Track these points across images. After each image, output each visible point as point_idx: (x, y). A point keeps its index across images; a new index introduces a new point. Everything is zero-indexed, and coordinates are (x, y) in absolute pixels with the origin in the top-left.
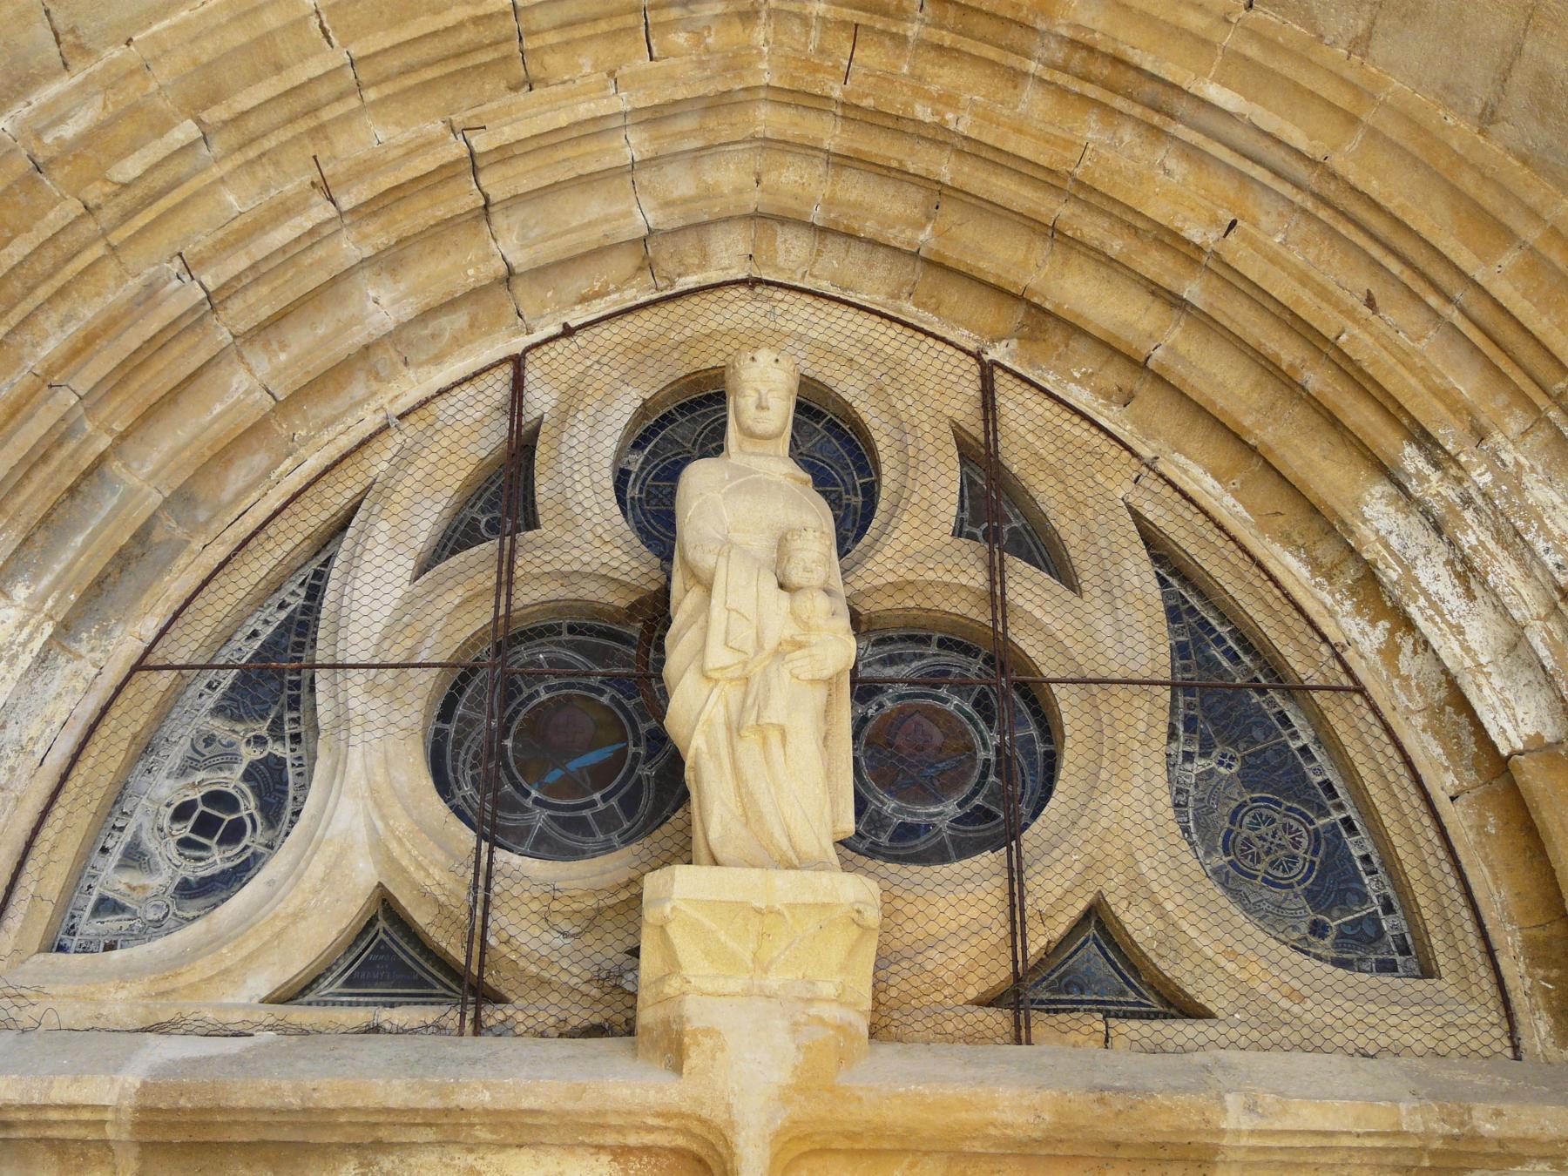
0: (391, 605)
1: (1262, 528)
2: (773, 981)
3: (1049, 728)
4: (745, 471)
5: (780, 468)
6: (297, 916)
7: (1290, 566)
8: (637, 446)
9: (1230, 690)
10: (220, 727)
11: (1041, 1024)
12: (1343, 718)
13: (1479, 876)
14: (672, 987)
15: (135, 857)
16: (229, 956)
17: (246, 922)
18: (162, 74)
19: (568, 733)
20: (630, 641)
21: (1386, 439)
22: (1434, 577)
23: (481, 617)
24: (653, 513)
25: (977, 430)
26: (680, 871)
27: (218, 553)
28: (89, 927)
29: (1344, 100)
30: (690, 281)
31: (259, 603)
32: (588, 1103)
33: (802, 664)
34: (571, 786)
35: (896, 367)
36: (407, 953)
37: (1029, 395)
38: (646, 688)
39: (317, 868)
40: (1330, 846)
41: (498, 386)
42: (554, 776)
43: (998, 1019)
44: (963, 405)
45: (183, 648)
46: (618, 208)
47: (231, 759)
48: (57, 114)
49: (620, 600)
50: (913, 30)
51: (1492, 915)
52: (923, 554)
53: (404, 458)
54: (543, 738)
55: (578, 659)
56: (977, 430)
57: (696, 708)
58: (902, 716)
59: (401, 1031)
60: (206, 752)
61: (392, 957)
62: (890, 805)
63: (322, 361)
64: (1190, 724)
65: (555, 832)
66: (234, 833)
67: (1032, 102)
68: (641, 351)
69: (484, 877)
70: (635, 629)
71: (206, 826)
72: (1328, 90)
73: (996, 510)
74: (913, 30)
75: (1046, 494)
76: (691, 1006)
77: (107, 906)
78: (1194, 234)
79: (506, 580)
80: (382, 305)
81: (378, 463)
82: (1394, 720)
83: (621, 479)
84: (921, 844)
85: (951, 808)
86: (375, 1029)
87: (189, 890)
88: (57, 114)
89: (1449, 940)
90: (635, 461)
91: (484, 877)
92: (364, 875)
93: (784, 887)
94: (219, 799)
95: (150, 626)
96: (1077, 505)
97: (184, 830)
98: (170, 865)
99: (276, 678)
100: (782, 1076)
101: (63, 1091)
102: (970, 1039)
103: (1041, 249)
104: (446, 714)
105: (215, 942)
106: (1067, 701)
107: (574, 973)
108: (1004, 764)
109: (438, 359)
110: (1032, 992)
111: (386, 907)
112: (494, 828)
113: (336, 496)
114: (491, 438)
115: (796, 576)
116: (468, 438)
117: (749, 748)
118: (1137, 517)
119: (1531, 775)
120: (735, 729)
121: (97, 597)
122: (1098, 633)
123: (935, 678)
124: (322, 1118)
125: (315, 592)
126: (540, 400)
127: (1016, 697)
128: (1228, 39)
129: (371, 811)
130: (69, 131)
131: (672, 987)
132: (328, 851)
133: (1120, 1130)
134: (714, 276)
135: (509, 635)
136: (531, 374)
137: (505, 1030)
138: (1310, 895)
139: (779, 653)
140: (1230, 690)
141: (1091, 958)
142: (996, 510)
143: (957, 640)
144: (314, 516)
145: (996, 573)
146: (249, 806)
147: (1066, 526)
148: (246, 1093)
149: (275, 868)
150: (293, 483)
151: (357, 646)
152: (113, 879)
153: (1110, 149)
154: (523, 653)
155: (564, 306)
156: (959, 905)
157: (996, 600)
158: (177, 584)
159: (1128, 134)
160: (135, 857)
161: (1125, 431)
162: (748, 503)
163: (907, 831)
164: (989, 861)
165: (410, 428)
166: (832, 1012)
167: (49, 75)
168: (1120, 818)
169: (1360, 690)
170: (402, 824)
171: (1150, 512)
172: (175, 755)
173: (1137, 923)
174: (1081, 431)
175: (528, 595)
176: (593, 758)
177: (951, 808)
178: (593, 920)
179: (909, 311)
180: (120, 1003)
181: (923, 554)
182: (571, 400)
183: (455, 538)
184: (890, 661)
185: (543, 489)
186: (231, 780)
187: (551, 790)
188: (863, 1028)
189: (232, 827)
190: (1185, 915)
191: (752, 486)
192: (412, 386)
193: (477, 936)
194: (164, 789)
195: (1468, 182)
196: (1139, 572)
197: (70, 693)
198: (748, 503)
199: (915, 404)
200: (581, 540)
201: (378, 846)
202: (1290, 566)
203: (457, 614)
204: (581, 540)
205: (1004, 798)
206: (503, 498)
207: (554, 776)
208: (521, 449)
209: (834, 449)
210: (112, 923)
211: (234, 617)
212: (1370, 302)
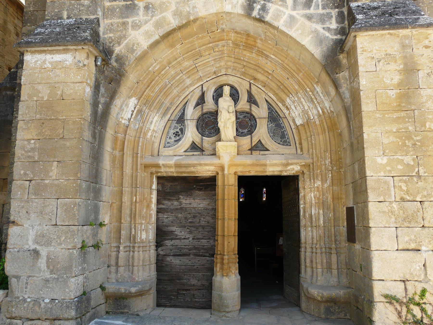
0: (192, 113)
1: (278, 101)
2: (228, 151)
3: (256, 122)
4: (225, 99)
5: (229, 99)
6: (185, 144)
7: (280, 105)
8: (215, 92)
9: (274, 118)
10: (176, 125)
11: (253, 152)
12: (285, 120)
13: (295, 136)
14: (219, 152)
15: (170, 138)
16: (180, 148)
17: (181, 145)
18: (165, 61)
19: (209, 124)
20: (215, 114)
21: (288, 93)
22: (293, 107)
23: (200, 113)
24: (217, 103)
25: (249, 90)
26: (219, 142)
27: (175, 108)
28: (167, 145)
29: (286, 56)
30: (219, 75)
31: (179, 112)
32: (212, 163)
33: (230, 121)
34: (210, 129)
35: (241, 83)
36: (196, 147)
37: (255, 86)
38: (216, 122)
39: (187, 140)
40: (283, 133)
41: (200, 87)
42: (208, 128)
43: (250, 152)
44: (248, 88)
45: (172, 118)
46: (211, 69)
47: (178, 128)
48: (155, 67)
49: (214, 111)
50: (241, 48)
51: (296, 140)
52: (243, 104)
53: (192, 96)
54: (207, 124)
55: (210, 116)
56: (249, 90)
57: (221, 125)
58: (242, 121)
59: (196, 155)
60: (175, 128)
61: (194, 147)
62: (240, 130)
63: (183, 88)
64: (270, 121)
65: (209, 134)
66: (179, 135)
67: (254, 55)
68: (215, 83)
69: (202, 139)
70: (215, 113)
71: (176, 135)
72: (284, 55)
73: (252, 100)
74: (241, 48)
75: (256, 97)
76: (220, 154)
77: (168, 143)
78: (270, 72)
79: (202, 110)
80: (188, 82)
81: (189, 97)
82: (289, 121)
83: (213, 96)
84: (243, 134)
85: (246, 130)
86: (193, 155)
87: (175, 141)
88: (155, 67)
89: (292, 143)
90: (215, 94)
91: (202, 139)
92: (191, 140)
93: (229, 143)
94: (177, 132)
95: (169, 116)
96: (259, 98)
97: (174, 135)
98: (173, 139)
99: (181, 119)
100: (229, 160)
101: (168, 163)
102: (247, 154)
103: (255, 71)
104: (197, 123)
105: (178, 147)
106: (257, 120)
107: (211, 149)
108: (251, 126)
109: (194, 85)
110: (252, 149)
111: (193, 142)
112: (203, 135)
113: (185, 101)
114: (200, 94)
115: (230, 111)
116: (198, 93)
117: (225, 129)
118: (265, 99)
119: (300, 128)
120: (224, 127)
121: (164, 114)
122: (261, 112)
123: (245, 117)
124: (190, 164)
125: (184, 110)
126: (205, 89)
127: (252, 118)
128: (274, 49)
129: (191, 134)
130: (156, 68)
131: (219, 152)
132: (188, 138)
133: (258, 163)
134: (222, 74)
135: (203, 115)
136: (203, 86)
137: (205, 155)
138: (281, 138)
139: (228, 120)
140: (274, 118)
141: (259, 145)
142: (252, 100)
143: (247, 113)
144: (183, 103)
145: (251, 106)
146: (180, 133)
147: (258, 100)
148: (183, 162)
149: (183, 139)
150: (181, 100)
151: (189, 118)
152: (169, 140)
153: (262, 61)
154: (205, 116)
155: (206, 78)
156: (246, 141)
157: (251, 109)
158: (171, 111)
159: (264, 59)
160: (170, 138)
161: (264, 90)
162: (226, 102)
163: (242, 133)
164: (249, 136)
165: (192, 93)
166: (233, 154)
167: (154, 63)
168: (262, 132)
169: (286, 118)
170: (194, 135)
171: (267, 98)
172: (173, 128)
173: (263, 142)
174: (260, 90)
175: (205, 111)
176: (212, 126)
177: (246, 130)
178: (212, 144)
179: (242, 77)
180: (171, 153)
181: (243, 104)
182: (208, 89)
183: (197, 104)
184: (241, 115)
185: (205, 99)
186: (178, 130)
187: (208, 130)
188: (236, 154)
189: (179, 134)
190: (268, 142)
191: (225, 101)
192: (192, 89)
193: (202, 145)
194: (172, 131)
195: (297, 66)
196: (265, 106)
197: (163, 124)
198: (226, 102)
199: (243, 87)
200: (209, 105)
201: (192, 137)
202: (280, 105)
203: (198, 113)
204: (209, 105)
205: (251, 129)
206: (201, 101)
207: (208, 128)
208: (203, 94)
209: (235, 95)
210: (169, 144)
211: (177, 114)
212: (288, 79)
